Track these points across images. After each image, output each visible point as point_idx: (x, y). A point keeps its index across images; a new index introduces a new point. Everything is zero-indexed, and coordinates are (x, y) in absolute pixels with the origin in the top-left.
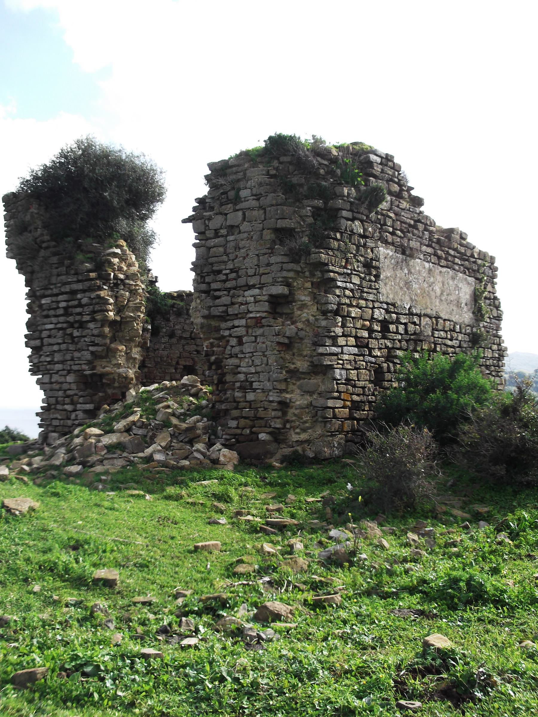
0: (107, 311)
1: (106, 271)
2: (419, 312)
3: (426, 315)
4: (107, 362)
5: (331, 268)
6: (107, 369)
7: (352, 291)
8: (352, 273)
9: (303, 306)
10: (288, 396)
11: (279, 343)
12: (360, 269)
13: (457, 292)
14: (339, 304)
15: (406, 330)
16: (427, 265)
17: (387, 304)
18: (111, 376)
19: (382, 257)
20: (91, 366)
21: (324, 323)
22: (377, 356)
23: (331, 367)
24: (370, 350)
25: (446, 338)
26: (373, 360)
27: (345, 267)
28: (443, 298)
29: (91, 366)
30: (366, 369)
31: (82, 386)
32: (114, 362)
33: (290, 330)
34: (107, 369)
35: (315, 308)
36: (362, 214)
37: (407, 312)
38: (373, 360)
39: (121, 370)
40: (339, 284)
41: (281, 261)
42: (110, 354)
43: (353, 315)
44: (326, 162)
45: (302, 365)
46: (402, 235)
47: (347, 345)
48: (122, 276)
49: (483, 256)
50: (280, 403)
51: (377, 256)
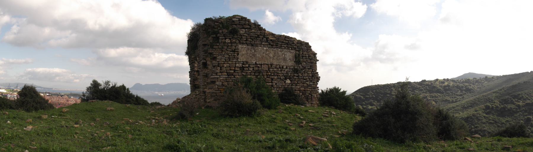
16: (265, 48)
19: (240, 49)
24: (234, 76)
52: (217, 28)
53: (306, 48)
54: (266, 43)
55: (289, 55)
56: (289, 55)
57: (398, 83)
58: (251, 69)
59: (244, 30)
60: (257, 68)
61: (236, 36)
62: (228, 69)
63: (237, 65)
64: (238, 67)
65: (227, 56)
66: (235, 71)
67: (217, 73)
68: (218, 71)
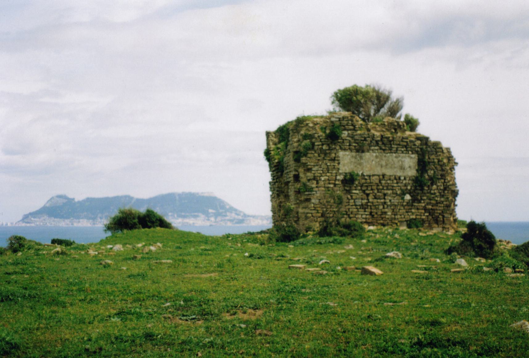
3: (373, 175)
5: (309, 163)
7: (322, 170)
16: (374, 154)
63: (338, 177)
64: (339, 180)
66: (335, 185)
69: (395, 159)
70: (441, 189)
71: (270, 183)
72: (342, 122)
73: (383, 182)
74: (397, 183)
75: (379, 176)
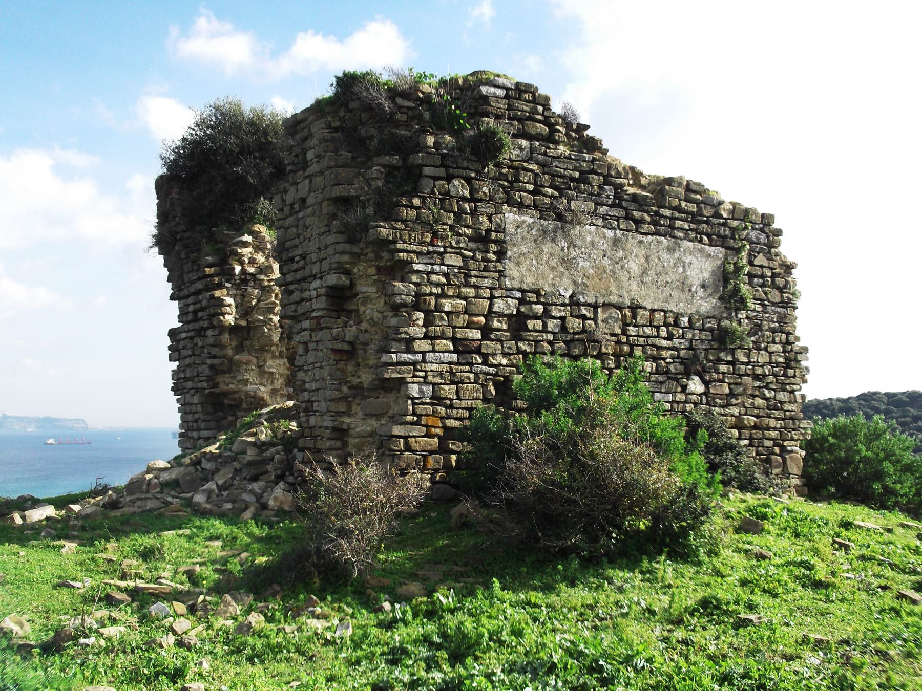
0: (223, 314)
1: (231, 265)
2: (591, 300)
3: (606, 305)
4: (232, 378)
5: (400, 246)
6: (231, 386)
7: (446, 275)
8: (445, 252)
9: (367, 300)
10: (347, 420)
11: (334, 350)
12: (462, 245)
13: (681, 269)
14: (418, 295)
15: (564, 328)
16: (610, 233)
17: (523, 291)
18: (236, 396)
19: (510, 228)
20: (211, 383)
21: (394, 321)
22: (500, 365)
23: (402, 382)
24: (485, 357)
25: (658, 336)
26: (492, 370)
27: (431, 244)
28: (647, 279)
29: (211, 383)
30: (476, 382)
31: (210, 408)
32: (240, 377)
33: (351, 332)
34: (231, 386)
35: (382, 301)
36: (467, 168)
37: (567, 301)
38: (492, 370)
39: (249, 388)
40: (417, 267)
41: (333, 241)
42: (234, 368)
43: (447, 309)
44: (411, 104)
45: (366, 378)
46: (556, 194)
47: (433, 351)
48: (251, 270)
49: (742, 214)
50: (334, 429)
51: (500, 226)
52: (407, 125)
53: (763, 237)
54: (614, 212)
55: (699, 263)
56: (699, 263)
57: (175, 352)
58: (552, 325)
59: (524, 143)
60: (574, 324)
61: (491, 169)
62: (461, 320)
63: (499, 305)
64: (500, 315)
65: (457, 261)
66: (487, 331)
67: (410, 340)
68: (417, 330)
69: (665, 256)
70: (777, 364)
71: (172, 333)
72: (517, 104)
73: (632, 330)
74: (670, 337)
75: (620, 308)
